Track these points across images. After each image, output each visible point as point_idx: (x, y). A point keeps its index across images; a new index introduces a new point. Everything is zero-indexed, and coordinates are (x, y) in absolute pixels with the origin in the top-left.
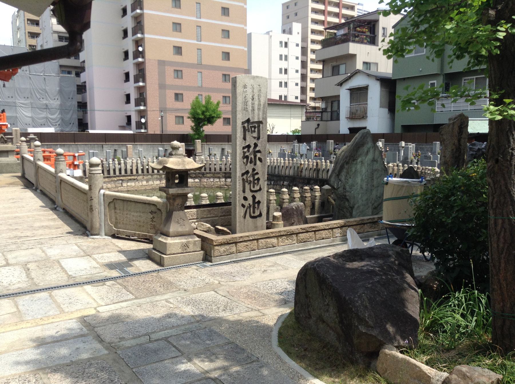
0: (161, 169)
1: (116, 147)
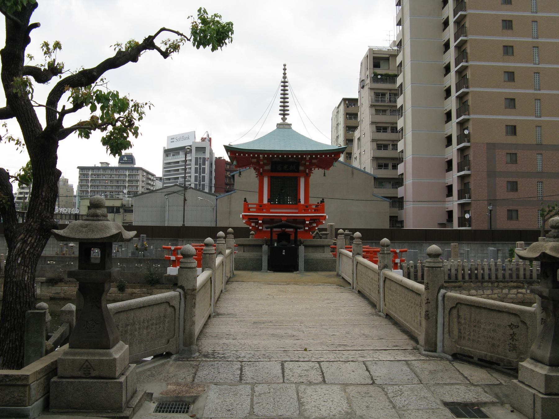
0: (536, 259)
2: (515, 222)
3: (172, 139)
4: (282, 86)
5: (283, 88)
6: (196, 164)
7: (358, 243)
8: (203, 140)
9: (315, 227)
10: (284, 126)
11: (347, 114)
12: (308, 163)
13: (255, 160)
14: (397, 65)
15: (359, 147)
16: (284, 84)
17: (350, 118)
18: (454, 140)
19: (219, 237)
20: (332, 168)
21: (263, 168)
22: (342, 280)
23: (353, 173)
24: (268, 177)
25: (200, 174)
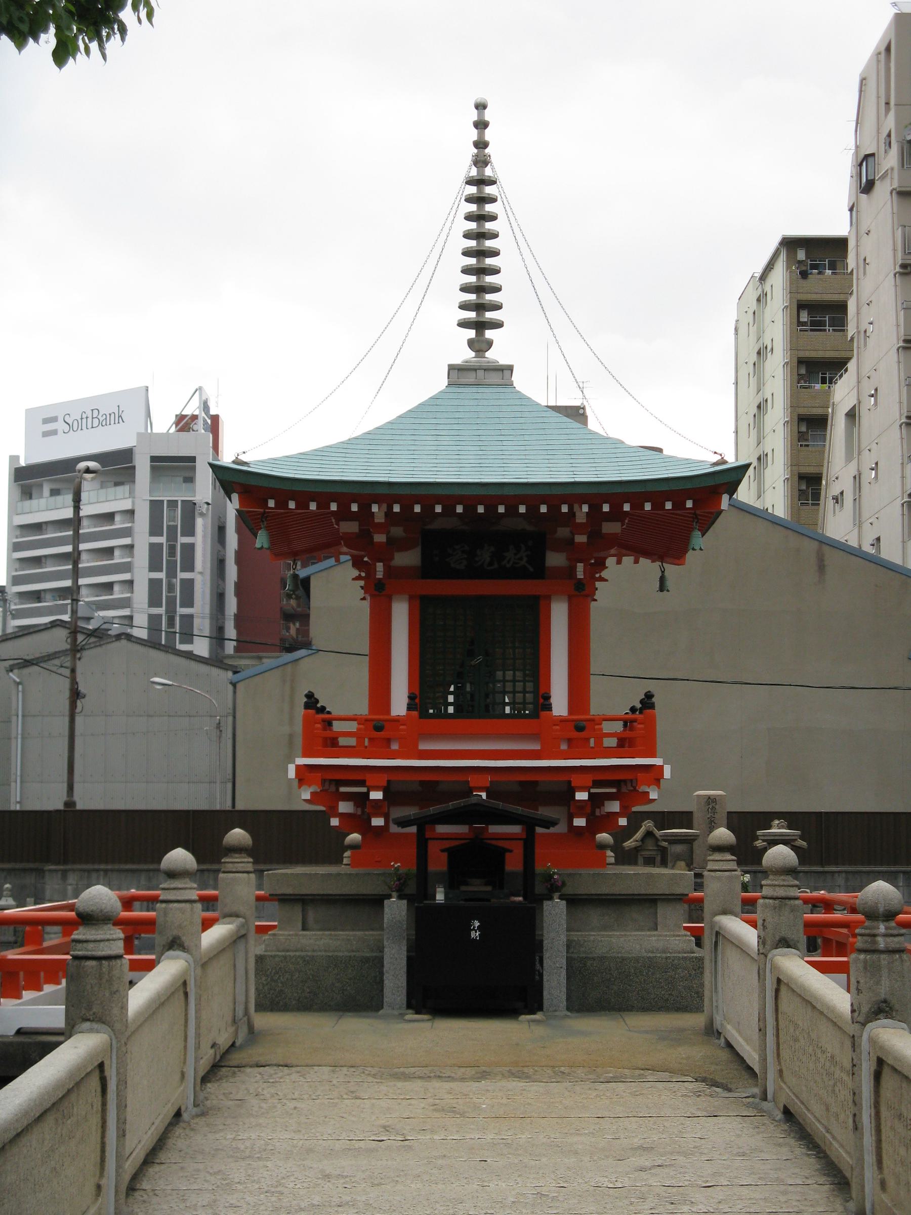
3: (47, 422)
4: (469, 200)
5: (473, 207)
6: (155, 530)
7: (781, 892)
8: (184, 423)
9: (616, 815)
10: (479, 375)
11: (801, 306)
12: (581, 539)
13: (351, 527)
15: (853, 449)
16: (481, 189)
17: (817, 325)
19: (172, 875)
20: (690, 555)
21: (387, 561)
22: (724, 1055)
23: (821, 567)
24: (411, 599)
25: (172, 574)
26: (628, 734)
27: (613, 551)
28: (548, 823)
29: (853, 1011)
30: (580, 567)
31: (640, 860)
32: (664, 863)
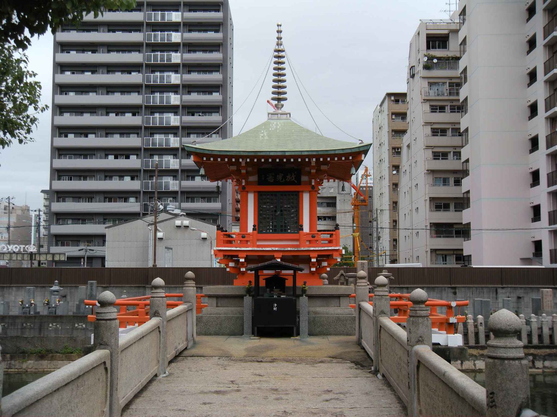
1: (520, 293)
2: (106, 253)
14: (460, 41)
16: (279, 55)
17: (397, 101)
18: (542, 143)
19: (156, 287)
24: (255, 192)
26: (331, 239)
27: (326, 177)
28: (301, 270)
29: (408, 341)
30: (313, 181)
31: (339, 283)
32: (347, 284)
